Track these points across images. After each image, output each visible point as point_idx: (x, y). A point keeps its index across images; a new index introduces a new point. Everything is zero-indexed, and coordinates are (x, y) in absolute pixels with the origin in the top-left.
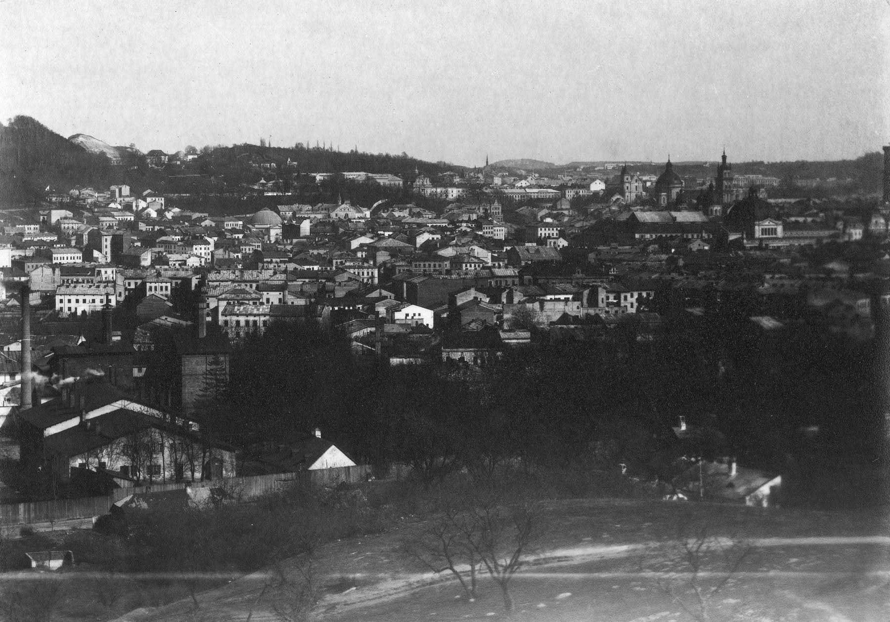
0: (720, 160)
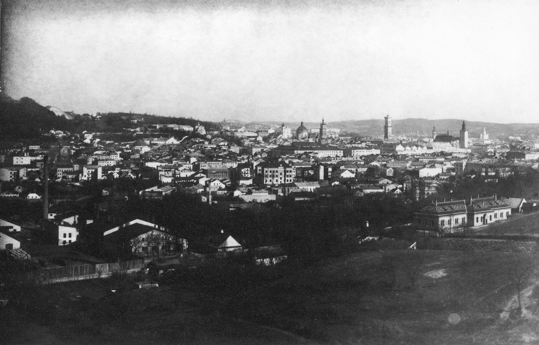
0: (322, 122)
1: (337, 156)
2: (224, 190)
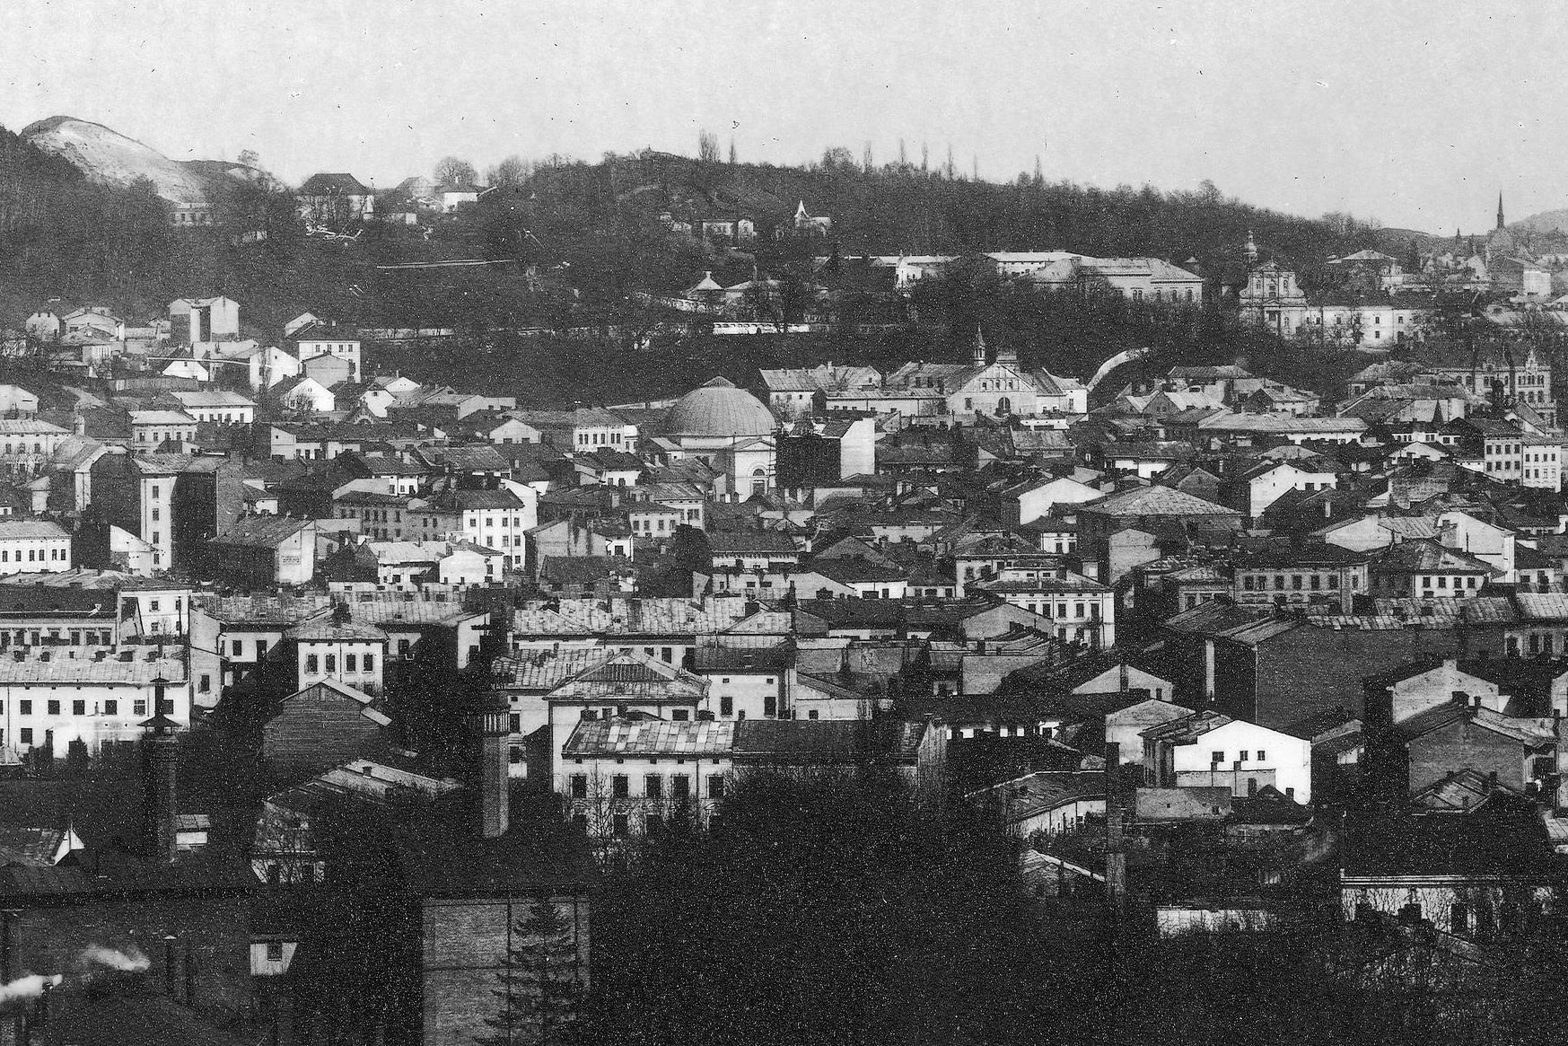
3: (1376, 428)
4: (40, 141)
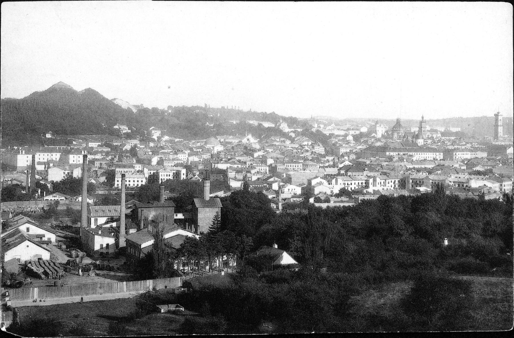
1: (434, 159)
2: (299, 197)
3: (301, 146)
4: (113, 101)
